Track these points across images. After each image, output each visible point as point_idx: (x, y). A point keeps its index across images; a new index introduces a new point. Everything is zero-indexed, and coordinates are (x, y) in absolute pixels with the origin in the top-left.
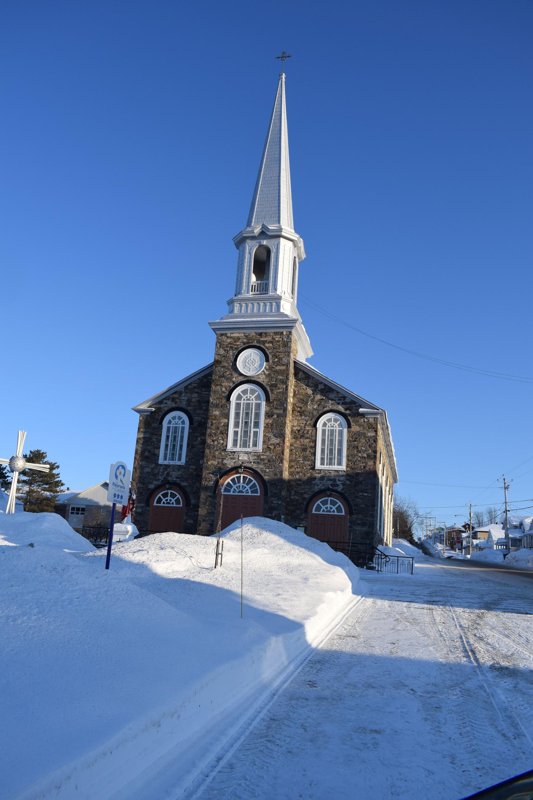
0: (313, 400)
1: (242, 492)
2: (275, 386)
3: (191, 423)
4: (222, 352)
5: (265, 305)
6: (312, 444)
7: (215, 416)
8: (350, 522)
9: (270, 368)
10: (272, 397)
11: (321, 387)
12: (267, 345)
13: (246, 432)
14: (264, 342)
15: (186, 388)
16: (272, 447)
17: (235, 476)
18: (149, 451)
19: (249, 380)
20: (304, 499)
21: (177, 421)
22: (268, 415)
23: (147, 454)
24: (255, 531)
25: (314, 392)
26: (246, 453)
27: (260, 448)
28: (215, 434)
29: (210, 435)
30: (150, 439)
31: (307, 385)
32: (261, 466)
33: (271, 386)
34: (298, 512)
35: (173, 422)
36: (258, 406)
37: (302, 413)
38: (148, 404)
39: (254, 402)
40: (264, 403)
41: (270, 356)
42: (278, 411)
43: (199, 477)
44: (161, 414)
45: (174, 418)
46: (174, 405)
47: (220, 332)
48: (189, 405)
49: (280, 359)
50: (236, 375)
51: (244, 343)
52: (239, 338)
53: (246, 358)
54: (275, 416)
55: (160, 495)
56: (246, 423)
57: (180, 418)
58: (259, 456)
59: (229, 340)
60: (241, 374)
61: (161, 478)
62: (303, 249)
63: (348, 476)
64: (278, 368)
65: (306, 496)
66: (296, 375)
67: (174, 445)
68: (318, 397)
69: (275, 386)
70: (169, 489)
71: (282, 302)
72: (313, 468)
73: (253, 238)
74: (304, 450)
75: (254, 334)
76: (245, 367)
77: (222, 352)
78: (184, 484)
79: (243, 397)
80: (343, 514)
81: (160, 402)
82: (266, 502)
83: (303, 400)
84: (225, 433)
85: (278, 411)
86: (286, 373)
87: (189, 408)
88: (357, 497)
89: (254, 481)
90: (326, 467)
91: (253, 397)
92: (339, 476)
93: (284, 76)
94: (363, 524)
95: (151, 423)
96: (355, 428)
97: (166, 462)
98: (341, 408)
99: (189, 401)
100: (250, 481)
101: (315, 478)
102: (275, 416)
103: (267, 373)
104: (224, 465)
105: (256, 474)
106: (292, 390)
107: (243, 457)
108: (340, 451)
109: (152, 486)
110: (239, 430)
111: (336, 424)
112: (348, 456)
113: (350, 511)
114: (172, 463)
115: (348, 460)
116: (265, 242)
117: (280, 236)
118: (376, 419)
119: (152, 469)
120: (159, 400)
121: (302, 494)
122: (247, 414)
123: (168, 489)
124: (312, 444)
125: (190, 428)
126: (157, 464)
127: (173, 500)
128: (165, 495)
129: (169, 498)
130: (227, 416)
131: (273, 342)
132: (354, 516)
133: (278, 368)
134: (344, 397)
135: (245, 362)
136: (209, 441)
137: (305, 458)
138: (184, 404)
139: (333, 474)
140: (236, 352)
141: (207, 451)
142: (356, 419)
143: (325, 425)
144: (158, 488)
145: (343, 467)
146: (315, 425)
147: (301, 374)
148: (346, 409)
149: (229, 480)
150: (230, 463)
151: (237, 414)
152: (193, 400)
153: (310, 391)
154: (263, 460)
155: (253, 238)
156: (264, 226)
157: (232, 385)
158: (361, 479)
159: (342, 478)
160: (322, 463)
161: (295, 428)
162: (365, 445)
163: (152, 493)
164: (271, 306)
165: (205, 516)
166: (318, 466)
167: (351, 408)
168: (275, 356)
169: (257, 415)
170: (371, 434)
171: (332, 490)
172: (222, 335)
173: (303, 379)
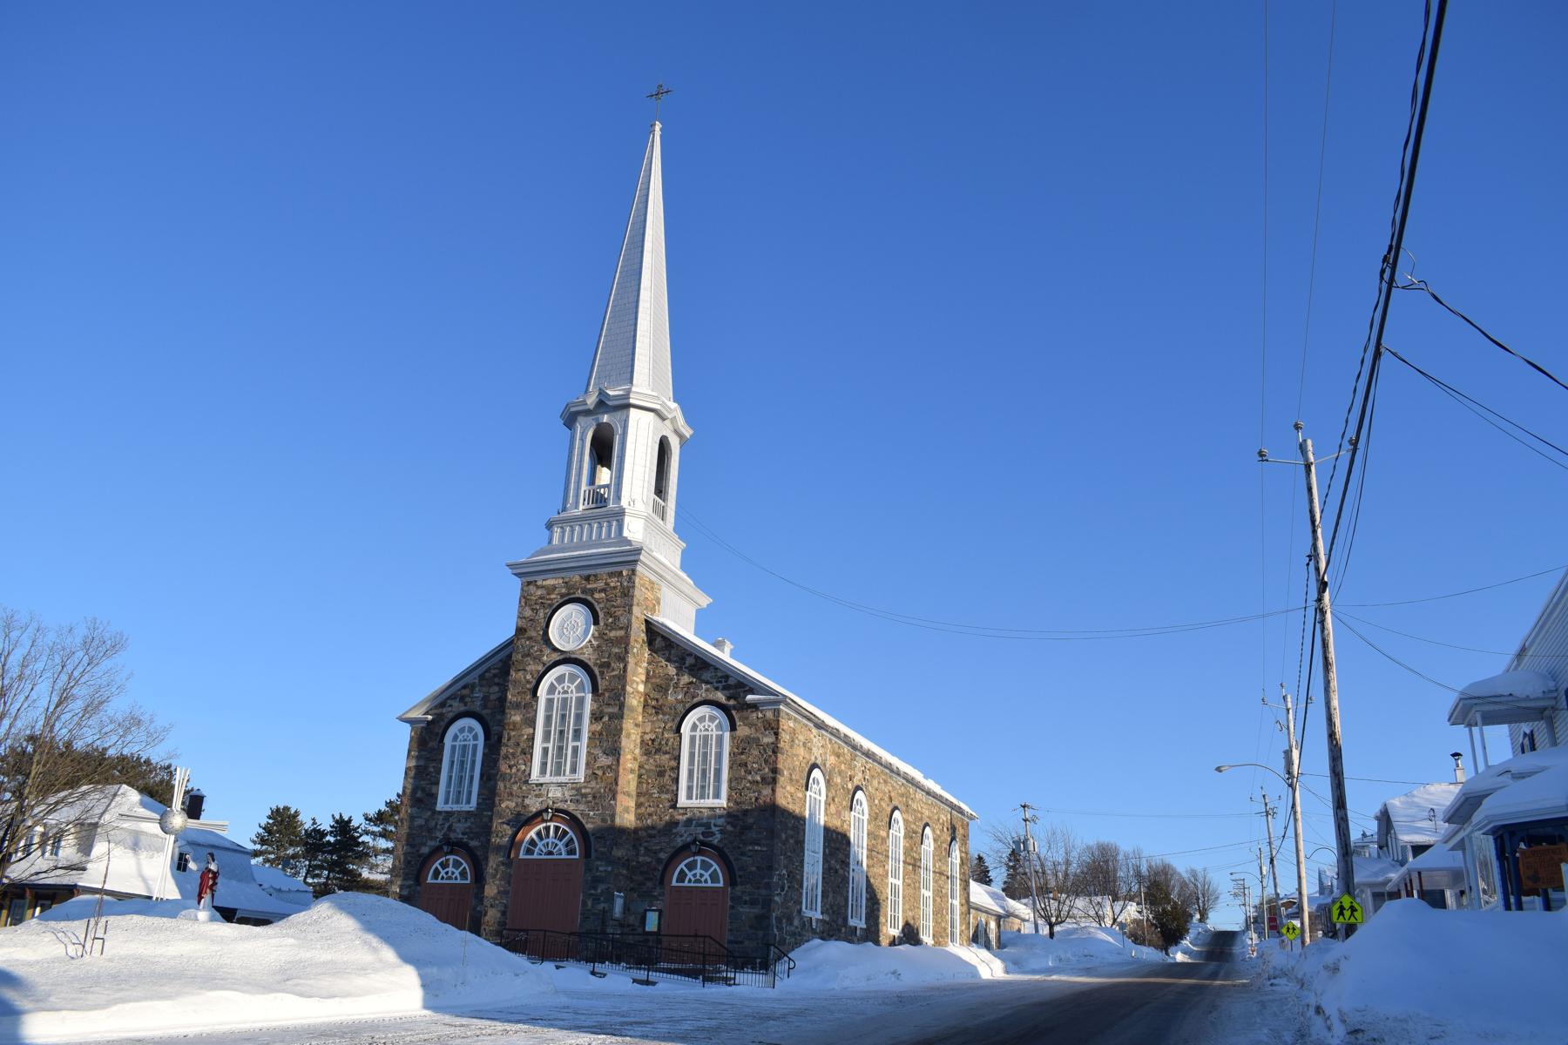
0: (676, 686)
1: (550, 853)
2: (607, 665)
3: (487, 737)
4: (528, 613)
5: (600, 527)
6: (673, 763)
7: (514, 724)
8: (732, 899)
9: (601, 636)
10: (602, 685)
11: (690, 661)
12: (597, 596)
13: (560, 749)
14: (592, 591)
15: (482, 677)
16: (600, 773)
17: (542, 826)
18: (423, 790)
19: (567, 659)
20: (659, 861)
21: (465, 734)
22: (596, 717)
23: (419, 794)
24: (330, 912)
25: (679, 669)
26: (560, 785)
27: (581, 776)
28: (513, 755)
29: (506, 757)
30: (426, 768)
31: (668, 660)
32: (582, 807)
33: (602, 665)
34: (649, 884)
35: (701, 726)
36: (581, 701)
37: (658, 710)
38: (424, 709)
39: (575, 695)
40: (589, 697)
41: (601, 615)
42: (610, 710)
43: (487, 830)
44: (443, 724)
45: (462, 730)
46: (463, 708)
47: (528, 575)
48: (485, 707)
49: (617, 618)
50: (547, 651)
51: (562, 596)
52: (554, 588)
53: (564, 621)
54: (606, 719)
55: (682, 866)
56: (562, 732)
57: (471, 730)
58: (579, 790)
59: (539, 592)
60: (555, 650)
61: (440, 835)
62: (681, 421)
63: (731, 816)
64: (613, 634)
65: (663, 856)
66: (650, 643)
67: (704, 771)
68: (686, 679)
69: (607, 665)
70: (451, 853)
71: (627, 519)
72: (674, 806)
73: (588, 413)
74: (661, 774)
75: (577, 578)
76: (562, 635)
77: (528, 613)
78: (473, 843)
79: (559, 689)
80: (721, 884)
81: (442, 705)
82: (589, 870)
83: (658, 686)
84: (528, 753)
85: (610, 710)
86: (624, 642)
87: (484, 712)
88: (743, 854)
89: (571, 834)
90: (695, 803)
91: (573, 687)
92: (715, 817)
93: (658, 127)
94: (753, 903)
95: (428, 741)
96: (743, 731)
97: (447, 808)
98: (720, 697)
99: (485, 699)
100: (565, 833)
101: (676, 823)
102: (606, 719)
103: (595, 643)
104: (525, 807)
105: (574, 821)
106: (641, 671)
107: (555, 793)
108: (718, 772)
109: (425, 850)
110: (550, 746)
111: (713, 726)
112: (730, 781)
113: (732, 880)
114: (456, 808)
115: (730, 788)
116: (605, 418)
117: (629, 406)
118: (777, 712)
119: (427, 821)
120: (439, 700)
121: (655, 852)
122: (563, 716)
123: (695, 854)
124: (673, 763)
125: (485, 745)
126: (434, 812)
127: (707, 875)
128: (691, 866)
129: (698, 871)
130: (532, 723)
131: (606, 585)
132: (739, 888)
133: (613, 634)
134: (727, 677)
135: (562, 627)
136: (504, 768)
137: (662, 789)
138: (476, 706)
139: (706, 813)
140: (549, 611)
141: (501, 785)
142: (745, 714)
143: (694, 727)
144: (436, 852)
145: (723, 802)
146: (678, 730)
147: (658, 642)
148: (729, 698)
149: (532, 834)
150: (534, 805)
151: (548, 719)
152: (492, 697)
153: (672, 670)
154: (584, 795)
155: (588, 413)
156: (602, 393)
157: (541, 668)
158: (751, 821)
159: (721, 821)
160: (689, 797)
161: (647, 737)
162: (758, 756)
163: (426, 861)
164: (610, 527)
165: (495, 899)
166: (683, 801)
167: (734, 696)
168: (609, 614)
169: (579, 717)
170: (768, 739)
171: (703, 843)
172: (529, 583)
173: (662, 649)
